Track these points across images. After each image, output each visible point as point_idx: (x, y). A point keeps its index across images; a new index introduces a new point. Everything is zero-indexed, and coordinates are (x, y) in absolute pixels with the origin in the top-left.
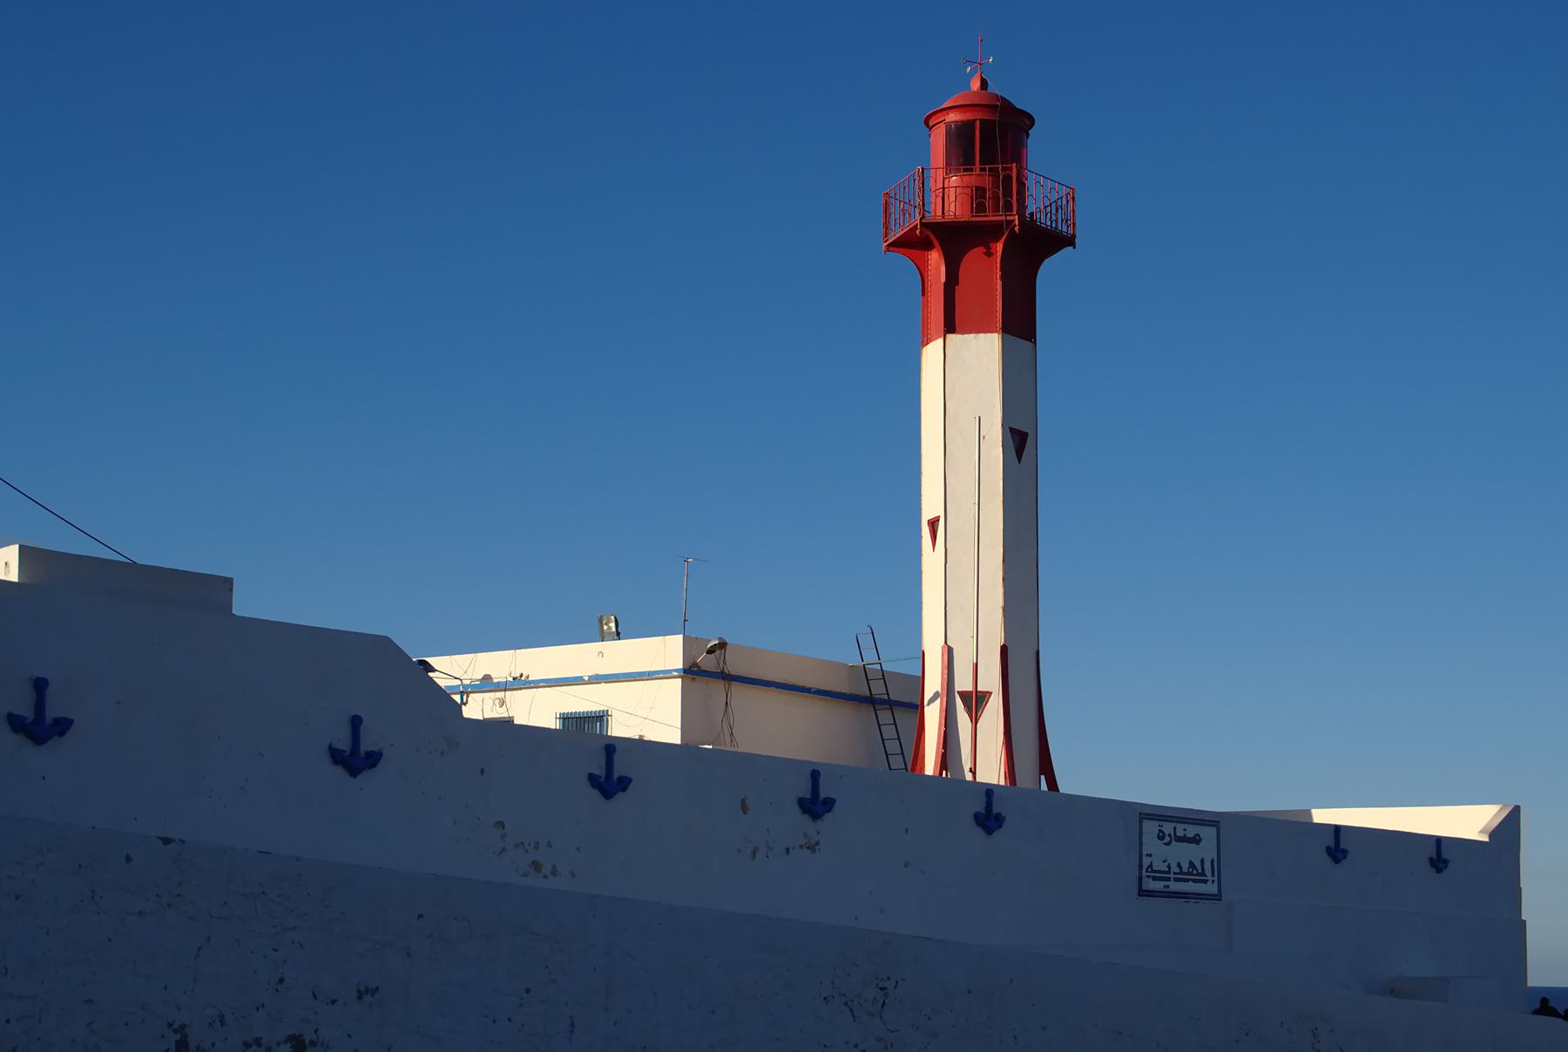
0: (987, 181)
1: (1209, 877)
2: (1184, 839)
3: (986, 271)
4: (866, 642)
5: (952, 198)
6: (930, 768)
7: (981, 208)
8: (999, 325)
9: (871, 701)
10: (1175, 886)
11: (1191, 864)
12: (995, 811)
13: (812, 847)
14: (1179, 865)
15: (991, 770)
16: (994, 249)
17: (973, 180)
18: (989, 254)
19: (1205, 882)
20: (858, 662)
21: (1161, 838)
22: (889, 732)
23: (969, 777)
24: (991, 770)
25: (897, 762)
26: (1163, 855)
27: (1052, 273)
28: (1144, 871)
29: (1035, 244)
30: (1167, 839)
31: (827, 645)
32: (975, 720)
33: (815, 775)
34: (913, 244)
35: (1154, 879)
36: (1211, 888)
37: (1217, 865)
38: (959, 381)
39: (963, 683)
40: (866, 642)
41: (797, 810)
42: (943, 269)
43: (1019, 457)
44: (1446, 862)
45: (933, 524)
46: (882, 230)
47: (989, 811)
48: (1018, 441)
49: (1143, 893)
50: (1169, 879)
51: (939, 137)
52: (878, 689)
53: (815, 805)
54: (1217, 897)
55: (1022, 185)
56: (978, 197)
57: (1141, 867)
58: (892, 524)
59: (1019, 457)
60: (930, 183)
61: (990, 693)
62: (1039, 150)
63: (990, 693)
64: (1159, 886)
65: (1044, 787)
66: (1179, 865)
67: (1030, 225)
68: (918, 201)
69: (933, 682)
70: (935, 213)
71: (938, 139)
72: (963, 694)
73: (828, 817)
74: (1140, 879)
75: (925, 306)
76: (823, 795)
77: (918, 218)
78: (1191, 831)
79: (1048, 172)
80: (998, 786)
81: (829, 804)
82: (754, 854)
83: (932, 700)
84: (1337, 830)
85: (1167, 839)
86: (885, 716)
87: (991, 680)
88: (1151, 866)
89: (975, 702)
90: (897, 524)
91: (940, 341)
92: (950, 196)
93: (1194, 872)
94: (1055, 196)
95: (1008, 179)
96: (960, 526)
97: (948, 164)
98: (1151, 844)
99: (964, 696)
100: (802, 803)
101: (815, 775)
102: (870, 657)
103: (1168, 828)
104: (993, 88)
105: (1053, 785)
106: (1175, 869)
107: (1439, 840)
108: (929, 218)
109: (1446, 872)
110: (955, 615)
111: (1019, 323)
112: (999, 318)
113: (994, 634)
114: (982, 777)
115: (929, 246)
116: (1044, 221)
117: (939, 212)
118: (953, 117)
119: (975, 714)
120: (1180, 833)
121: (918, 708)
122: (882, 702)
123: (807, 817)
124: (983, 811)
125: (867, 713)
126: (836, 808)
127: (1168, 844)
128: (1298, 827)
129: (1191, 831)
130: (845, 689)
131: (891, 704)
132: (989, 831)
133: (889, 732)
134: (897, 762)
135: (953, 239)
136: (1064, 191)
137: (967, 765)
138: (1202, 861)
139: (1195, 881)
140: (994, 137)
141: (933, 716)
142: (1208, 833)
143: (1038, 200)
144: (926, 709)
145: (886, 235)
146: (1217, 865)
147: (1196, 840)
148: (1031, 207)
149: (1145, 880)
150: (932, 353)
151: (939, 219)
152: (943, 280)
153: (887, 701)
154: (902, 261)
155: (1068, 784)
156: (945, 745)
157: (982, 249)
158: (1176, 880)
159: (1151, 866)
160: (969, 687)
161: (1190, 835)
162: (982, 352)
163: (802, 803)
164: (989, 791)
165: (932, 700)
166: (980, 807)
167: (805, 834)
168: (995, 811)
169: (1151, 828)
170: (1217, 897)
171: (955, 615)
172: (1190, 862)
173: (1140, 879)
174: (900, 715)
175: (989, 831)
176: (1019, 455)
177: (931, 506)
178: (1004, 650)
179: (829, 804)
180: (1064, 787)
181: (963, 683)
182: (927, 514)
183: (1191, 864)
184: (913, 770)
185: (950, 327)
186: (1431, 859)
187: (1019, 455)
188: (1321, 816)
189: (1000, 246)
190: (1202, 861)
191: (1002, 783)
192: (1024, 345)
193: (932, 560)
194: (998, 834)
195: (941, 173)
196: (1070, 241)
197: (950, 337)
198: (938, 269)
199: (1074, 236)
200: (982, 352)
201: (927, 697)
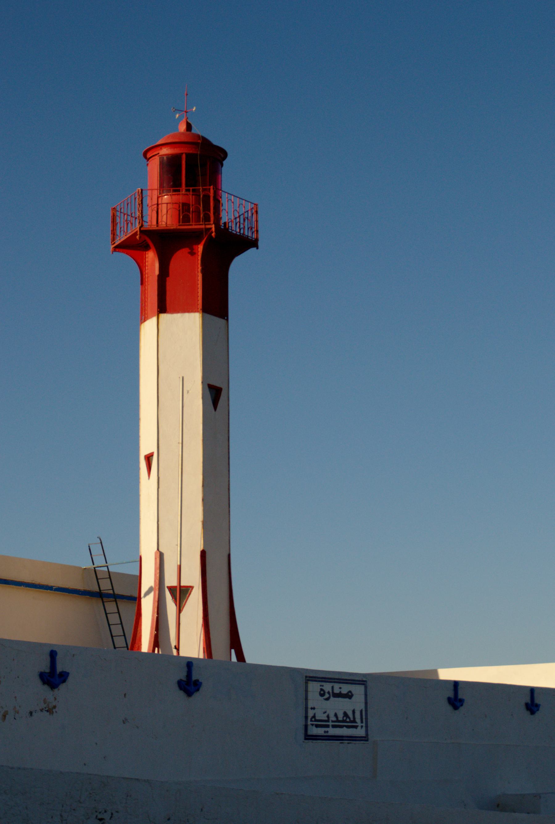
0: (191, 199)
1: (359, 724)
2: (339, 695)
3: (190, 266)
4: (97, 550)
5: (164, 211)
6: (145, 646)
7: (186, 220)
8: (200, 307)
9: (100, 595)
10: (333, 731)
11: (345, 714)
12: (194, 678)
13: (50, 710)
14: (336, 715)
15: (192, 646)
16: (195, 249)
17: (180, 198)
18: (193, 253)
19: (356, 727)
20: (89, 565)
21: (322, 695)
22: (114, 619)
23: (175, 652)
24: (192, 646)
25: (120, 641)
26: (322, 708)
27: (240, 269)
28: (309, 720)
29: (229, 245)
30: (327, 696)
31: (67, 553)
32: (180, 611)
33: (53, 655)
34: (133, 246)
35: (317, 726)
36: (360, 732)
37: (365, 714)
38: (169, 349)
39: (171, 580)
40: (97, 550)
41: (176, 687)
42: (157, 265)
43: (215, 408)
44: (461, 701)
45: (149, 458)
46: (110, 236)
47: (189, 679)
48: (215, 394)
49: (308, 737)
50: (328, 726)
51: (155, 165)
52: (105, 586)
53: (53, 678)
54: (365, 739)
55: (218, 203)
56: (183, 212)
57: (306, 717)
58: (119, 460)
59: (215, 408)
60: (147, 201)
61: (192, 587)
62: (230, 176)
63: (192, 587)
64: (320, 731)
65: (234, 659)
66: (336, 715)
67: (224, 232)
68: (138, 214)
69: (148, 580)
70: (150, 223)
71: (154, 168)
72: (171, 589)
73: (63, 687)
74: (306, 727)
75: (144, 293)
76: (59, 669)
77: (138, 226)
78: (345, 689)
79: (237, 192)
80: (198, 659)
81: (64, 676)
82: (4, 716)
83: (147, 593)
84: (456, 684)
85: (327, 696)
86: (111, 607)
87: (192, 577)
88: (314, 716)
89: (181, 594)
90: (122, 460)
91: (154, 319)
92: (162, 210)
93: (347, 721)
94: (242, 211)
95: (206, 198)
96: (169, 460)
97: (161, 186)
98: (315, 700)
99: (172, 589)
100: (42, 676)
101: (53, 655)
102: (99, 561)
103: (327, 687)
104: (195, 130)
105: (241, 657)
106: (333, 718)
107: (532, 690)
108: (146, 226)
109: (538, 714)
110: (164, 530)
111: (215, 305)
112: (200, 302)
113: (195, 542)
114: (183, 653)
115: (147, 248)
116: (235, 228)
117: (154, 222)
118: (165, 151)
119: (180, 603)
120: (337, 691)
121: (137, 600)
122: (108, 596)
123: (46, 687)
124: (48, 670)
125: (97, 604)
126: (70, 679)
127: (327, 699)
128: (426, 683)
129: (345, 689)
130: (79, 586)
131: (116, 597)
132: (189, 694)
133: (114, 619)
134: (120, 641)
135: (163, 242)
136: (249, 206)
137: (173, 643)
138: (354, 712)
139: (348, 727)
140: (195, 166)
141: (148, 605)
142: (358, 690)
143: (229, 213)
144: (144, 601)
145: (113, 239)
146: (365, 714)
147: (349, 696)
148: (225, 218)
149: (310, 727)
150: (148, 328)
151: (154, 227)
152: (157, 272)
153: (112, 595)
154: (125, 260)
155: (252, 656)
156: (157, 629)
157: (185, 251)
158: (334, 726)
159: (314, 716)
160: (174, 583)
161: (344, 691)
162: (187, 327)
163: (42, 676)
164: (190, 663)
165: (147, 593)
166: (182, 675)
167: (45, 701)
168: (194, 678)
169: (314, 687)
170: (365, 739)
171: (164, 530)
172: (338, 712)
173: (306, 727)
174: (124, 607)
175: (189, 694)
176: (215, 403)
177: (147, 444)
178: (203, 554)
179: (64, 676)
180: (250, 658)
181: (171, 580)
182: (144, 451)
183: (345, 714)
184: (132, 649)
185: (162, 309)
186: (527, 704)
187: (215, 403)
188: (447, 674)
189: (200, 248)
190: (354, 712)
191: (201, 656)
192: (220, 322)
193: (147, 486)
194: (197, 696)
195: (156, 193)
196: (254, 244)
197: (162, 316)
198: (153, 265)
199: (257, 240)
200: (187, 327)
201: (144, 590)
